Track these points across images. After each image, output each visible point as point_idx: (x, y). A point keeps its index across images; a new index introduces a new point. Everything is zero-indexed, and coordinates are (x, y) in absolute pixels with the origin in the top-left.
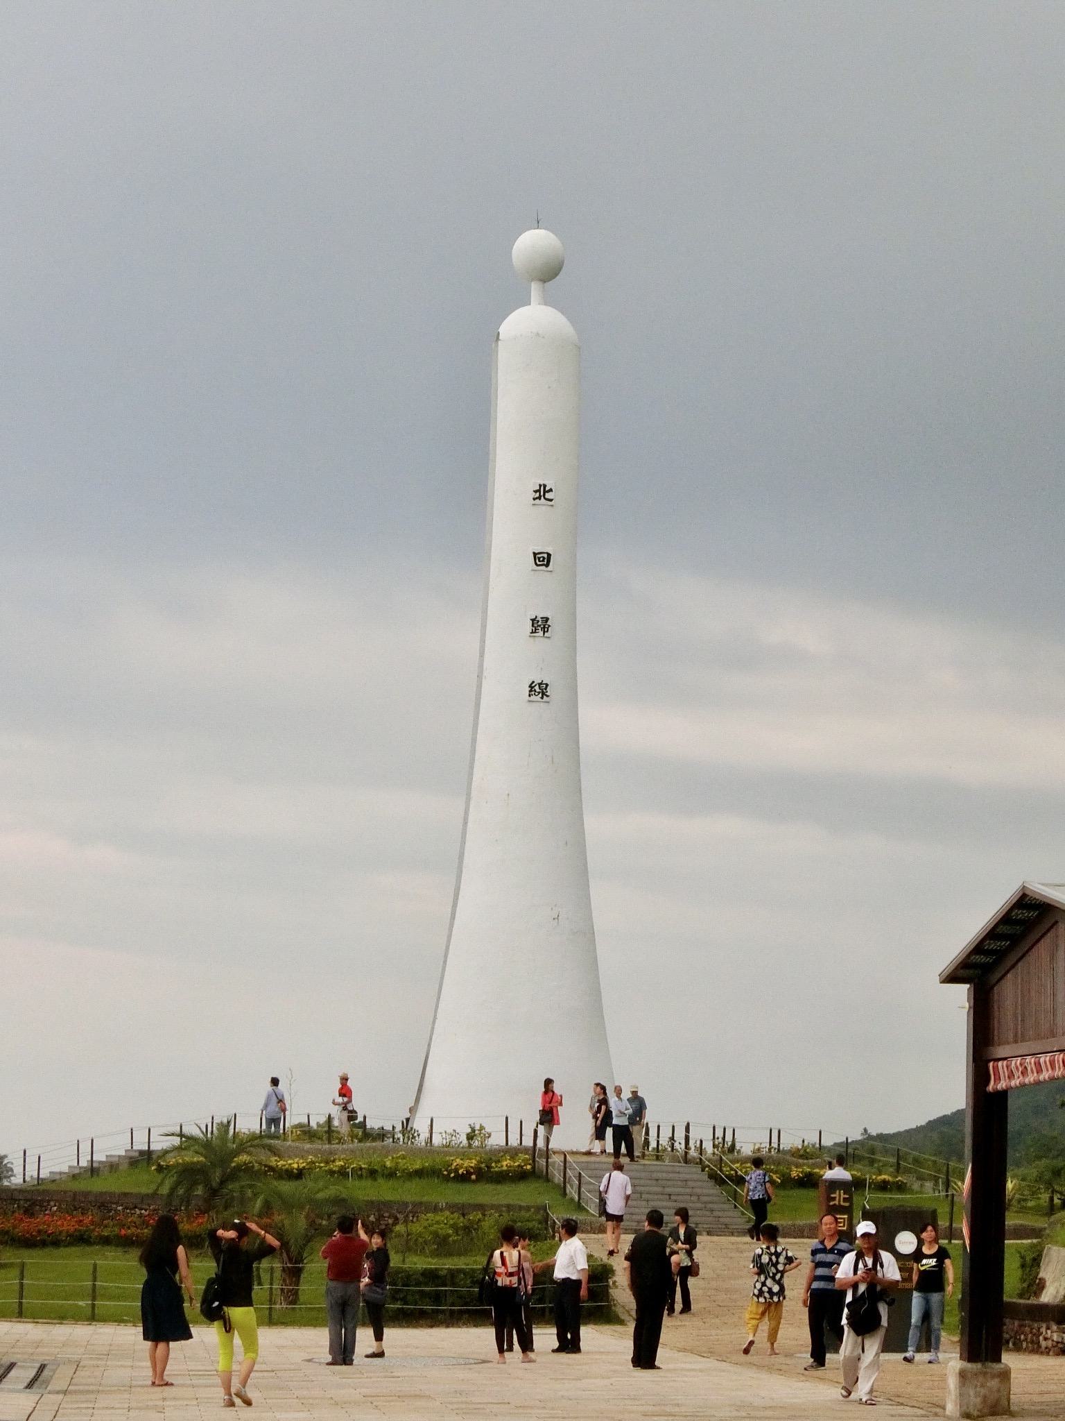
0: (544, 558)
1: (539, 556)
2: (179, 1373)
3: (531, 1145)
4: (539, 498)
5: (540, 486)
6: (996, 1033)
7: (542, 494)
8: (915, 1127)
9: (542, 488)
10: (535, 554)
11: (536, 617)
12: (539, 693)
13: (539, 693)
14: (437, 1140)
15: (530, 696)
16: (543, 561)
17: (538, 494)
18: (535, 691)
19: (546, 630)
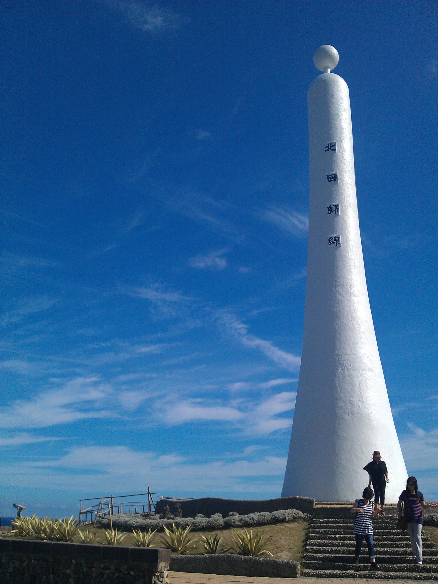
0: (333, 177)
1: (330, 177)
2: (279, 513)
3: (85, 519)
4: (328, 150)
5: (328, 144)
6: (177, 501)
7: (330, 147)
8: (399, 499)
9: (329, 145)
10: (328, 176)
11: (331, 206)
12: (334, 243)
13: (334, 243)
14: (418, 534)
15: (329, 245)
16: (333, 178)
17: (327, 148)
18: (332, 242)
19: (336, 211)
